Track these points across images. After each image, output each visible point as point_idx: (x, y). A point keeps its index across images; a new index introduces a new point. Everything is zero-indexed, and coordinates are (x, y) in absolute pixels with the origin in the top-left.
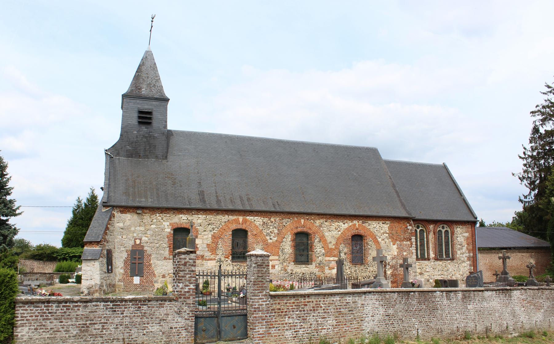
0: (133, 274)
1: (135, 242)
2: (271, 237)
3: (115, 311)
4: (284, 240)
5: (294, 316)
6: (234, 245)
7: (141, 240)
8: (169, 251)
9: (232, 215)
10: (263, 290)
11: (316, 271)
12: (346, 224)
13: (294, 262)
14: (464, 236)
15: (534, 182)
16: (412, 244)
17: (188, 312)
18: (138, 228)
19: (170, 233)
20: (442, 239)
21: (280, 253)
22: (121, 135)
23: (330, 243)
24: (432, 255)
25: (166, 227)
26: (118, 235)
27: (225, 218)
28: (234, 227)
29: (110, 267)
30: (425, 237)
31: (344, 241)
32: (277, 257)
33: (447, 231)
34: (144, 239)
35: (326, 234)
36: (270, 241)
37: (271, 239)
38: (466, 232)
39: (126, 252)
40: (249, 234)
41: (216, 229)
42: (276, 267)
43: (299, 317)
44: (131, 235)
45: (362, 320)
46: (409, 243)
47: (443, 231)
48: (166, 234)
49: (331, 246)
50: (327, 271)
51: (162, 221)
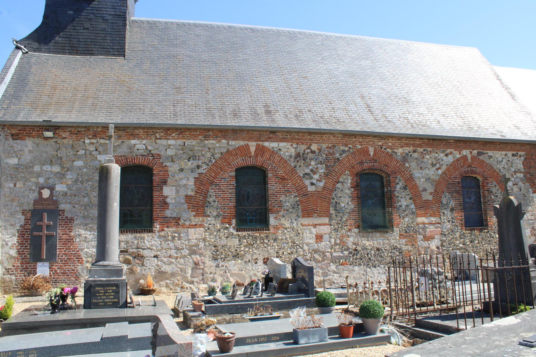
0: (37, 258)
1: (40, 194)
2: (314, 181)
4: (339, 185)
6: (241, 198)
7: (52, 189)
9: (234, 139)
11: (403, 244)
12: (450, 157)
13: (358, 227)
21: (332, 211)
22: (45, 17)
23: (425, 190)
26: (6, 181)
27: (221, 145)
28: (239, 162)
31: (448, 188)
32: (326, 220)
34: (60, 188)
37: (312, 184)
39: (23, 213)
40: (270, 175)
41: (205, 167)
42: (326, 237)
44: (33, 180)
49: (427, 196)
50: (421, 243)
51: (95, 153)
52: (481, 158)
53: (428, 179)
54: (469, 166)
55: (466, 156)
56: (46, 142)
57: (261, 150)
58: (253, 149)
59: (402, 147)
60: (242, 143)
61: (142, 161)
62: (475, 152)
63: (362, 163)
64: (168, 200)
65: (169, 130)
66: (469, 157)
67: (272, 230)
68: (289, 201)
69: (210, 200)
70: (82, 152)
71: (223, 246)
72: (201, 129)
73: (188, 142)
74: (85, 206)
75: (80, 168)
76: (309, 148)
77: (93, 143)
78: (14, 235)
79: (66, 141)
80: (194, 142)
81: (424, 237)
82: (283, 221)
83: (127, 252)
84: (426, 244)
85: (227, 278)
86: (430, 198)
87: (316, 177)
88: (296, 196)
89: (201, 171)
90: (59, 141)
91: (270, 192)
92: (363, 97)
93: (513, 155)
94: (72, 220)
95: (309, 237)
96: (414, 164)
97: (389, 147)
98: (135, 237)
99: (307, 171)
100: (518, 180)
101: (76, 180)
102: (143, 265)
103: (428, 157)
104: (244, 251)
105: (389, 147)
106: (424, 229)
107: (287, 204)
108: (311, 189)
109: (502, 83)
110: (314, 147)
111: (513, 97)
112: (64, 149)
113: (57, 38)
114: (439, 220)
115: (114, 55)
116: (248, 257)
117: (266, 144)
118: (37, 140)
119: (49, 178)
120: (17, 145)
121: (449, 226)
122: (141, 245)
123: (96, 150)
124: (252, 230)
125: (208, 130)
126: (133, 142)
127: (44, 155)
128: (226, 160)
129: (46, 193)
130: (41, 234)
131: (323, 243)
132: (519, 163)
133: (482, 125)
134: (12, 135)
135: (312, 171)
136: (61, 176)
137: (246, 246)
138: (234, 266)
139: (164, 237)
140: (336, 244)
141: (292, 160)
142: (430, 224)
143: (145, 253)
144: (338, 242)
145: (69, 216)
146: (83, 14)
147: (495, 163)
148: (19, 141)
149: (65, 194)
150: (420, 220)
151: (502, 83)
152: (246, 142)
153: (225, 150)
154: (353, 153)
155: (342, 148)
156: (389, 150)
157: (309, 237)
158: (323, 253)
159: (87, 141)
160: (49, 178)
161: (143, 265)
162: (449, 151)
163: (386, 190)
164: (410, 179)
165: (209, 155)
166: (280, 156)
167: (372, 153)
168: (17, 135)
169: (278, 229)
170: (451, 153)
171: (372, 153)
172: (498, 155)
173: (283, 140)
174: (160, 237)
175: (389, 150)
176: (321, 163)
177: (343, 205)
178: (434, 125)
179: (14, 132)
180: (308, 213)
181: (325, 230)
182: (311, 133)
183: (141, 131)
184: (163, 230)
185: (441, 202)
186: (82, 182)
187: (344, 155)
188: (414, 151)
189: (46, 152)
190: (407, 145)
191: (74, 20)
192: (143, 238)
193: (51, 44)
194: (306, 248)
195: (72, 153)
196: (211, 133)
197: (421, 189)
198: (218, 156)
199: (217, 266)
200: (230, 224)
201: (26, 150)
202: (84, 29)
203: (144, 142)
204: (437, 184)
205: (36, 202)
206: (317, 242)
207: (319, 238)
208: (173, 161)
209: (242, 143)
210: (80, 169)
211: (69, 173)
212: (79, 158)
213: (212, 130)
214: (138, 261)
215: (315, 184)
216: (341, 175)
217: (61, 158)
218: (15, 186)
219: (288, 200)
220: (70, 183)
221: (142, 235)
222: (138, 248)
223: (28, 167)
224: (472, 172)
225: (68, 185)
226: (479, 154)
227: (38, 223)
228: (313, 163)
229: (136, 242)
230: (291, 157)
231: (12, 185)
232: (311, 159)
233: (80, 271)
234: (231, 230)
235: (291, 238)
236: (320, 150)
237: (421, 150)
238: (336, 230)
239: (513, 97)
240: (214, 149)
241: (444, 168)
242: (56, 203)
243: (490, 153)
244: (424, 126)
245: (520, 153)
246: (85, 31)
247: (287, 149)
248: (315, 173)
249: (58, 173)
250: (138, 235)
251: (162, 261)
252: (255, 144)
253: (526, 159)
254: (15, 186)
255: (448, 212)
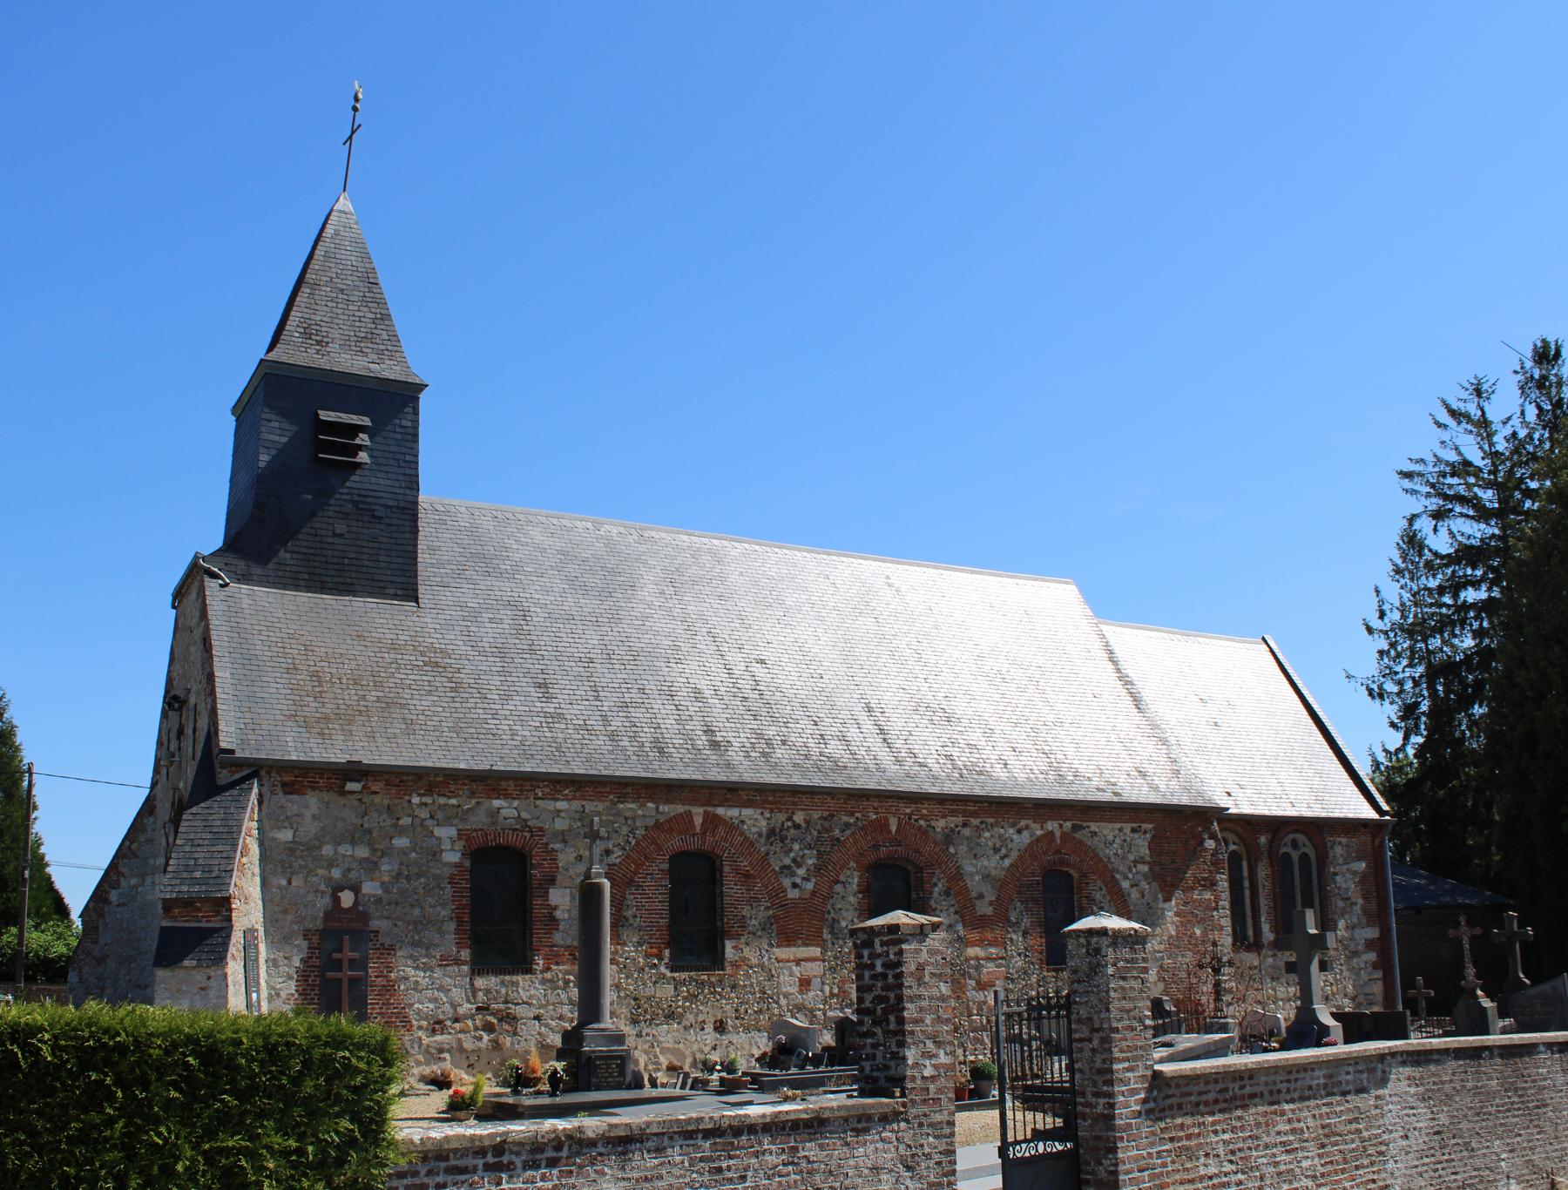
1: (337, 900)
2: (798, 881)
3: (719, 1170)
4: (838, 888)
5: (1221, 1151)
7: (356, 889)
8: (458, 931)
9: (668, 802)
10: (1135, 1058)
12: (1025, 834)
14: (1355, 873)
15: (1417, 705)
16: (1217, 899)
17: (937, 1158)
18: (346, 850)
19: (456, 865)
20: (1293, 881)
21: (827, 936)
23: (981, 896)
24: (1268, 935)
25: (446, 845)
27: (648, 812)
28: (675, 843)
29: (254, 996)
30: (1246, 874)
31: (1019, 892)
32: (816, 951)
33: (1304, 857)
34: (369, 888)
35: (968, 868)
36: (793, 894)
37: (795, 885)
38: (1360, 859)
40: (727, 869)
42: (816, 982)
43: (1233, 1152)
44: (321, 872)
45: (1381, 1153)
46: (1208, 895)
47: (1295, 856)
48: (447, 872)
49: (984, 908)
51: (429, 823)
52: (1077, 835)
53: (986, 877)
54: (1058, 852)
55: (1052, 833)
56: (342, 801)
57: (712, 822)
58: (698, 821)
59: (944, 816)
60: (680, 809)
61: (511, 839)
62: (1068, 824)
63: (876, 847)
64: (558, 914)
65: (560, 784)
66: (1058, 834)
67: (729, 970)
68: (756, 915)
69: (629, 913)
70: (406, 821)
71: (649, 999)
72: (612, 783)
73: (590, 806)
74: (416, 923)
75: (404, 852)
76: (790, 819)
77: (426, 804)
78: (290, 978)
79: (377, 799)
80: (601, 806)
81: (978, 982)
82: (747, 952)
83: (487, 1009)
84: (980, 996)
85: (656, 1056)
86: (989, 911)
87: (801, 872)
88: (767, 908)
89: (612, 859)
90: (367, 799)
91: (727, 900)
92: (869, 709)
93: (1133, 830)
94: (392, 948)
95: (788, 983)
96: (963, 848)
97: (922, 817)
98: (502, 982)
99: (787, 861)
100: (1139, 877)
101: (399, 875)
102: (515, 1034)
103: (987, 834)
104: (683, 1007)
105: (922, 817)
106: (978, 968)
107: (754, 922)
108: (793, 894)
109: (1118, 670)
110: (799, 818)
111: (1137, 701)
112: (375, 815)
113: (282, 554)
114: (1003, 953)
115: (395, 597)
116: (690, 1018)
117: (720, 811)
118: (326, 796)
119: (349, 870)
120: (292, 804)
121: (1019, 962)
122: (513, 995)
123: (432, 817)
124: (697, 969)
125: (626, 785)
126: (496, 803)
127: (340, 824)
128: (654, 842)
129: (347, 899)
130: (340, 975)
131: (812, 994)
132: (1142, 846)
133: (1082, 768)
134: (284, 785)
135: (794, 860)
136: (371, 866)
137: (685, 999)
138: (667, 1033)
139: (550, 981)
140: (832, 995)
141: (763, 840)
142: (988, 959)
143: (520, 1011)
144: (836, 991)
145: (388, 942)
146: (332, 502)
147: (1102, 845)
148: (294, 797)
149: (379, 900)
150: (972, 951)
151: (1118, 670)
152: (687, 808)
153: (651, 822)
154: (863, 828)
155: (845, 819)
156: (922, 822)
157: (788, 983)
158: (811, 1011)
159: (416, 800)
160: (349, 870)
161: (515, 1034)
162: (1023, 823)
163: (914, 895)
164: (957, 877)
165: (625, 830)
166: (742, 834)
167: (894, 829)
168: (293, 783)
169: (738, 967)
170: (1027, 827)
171: (894, 829)
172: (1107, 830)
173: (748, 804)
174: (544, 981)
175: (922, 822)
176: (810, 847)
177: (844, 924)
178: (999, 772)
179: (286, 779)
180: (788, 938)
181: (815, 969)
182: (795, 791)
183: (511, 783)
184: (549, 969)
185: (1008, 920)
186: (408, 878)
187: (848, 832)
188: (965, 825)
189: (343, 820)
190: (954, 813)
191: (313, 515)
192: (516, 984)
193: (271, 566)
194: (783, 1001)
195: (389, 822)
196: (629, 790)
197: (974, 894)
198: (640, 832)
199: (639, 1035)
200: (661, 959)
201: (308, 814)
202: (336, 535)
203: (516, 803)
204: (1001, 885)
205: (328, 915)
206: (801, 992)
207: (805, 984)
208: (565, 841)
209: (680, 809)
210: (405, 853)
211: (385, 860)
212: (402, 831)
213: (632, 784)
214: (506, 1027)
215: (799, 886)
216: (842, 868)
217: (370, 832)
218: (289, 883)
219: (756, 915)
220: (386, 879)
221: (515, 978)
222: (506, 1002)
223: (312, 847)
224: (1062, 862)
225: (383, 884)
226: (1075, 828)
227: (336, 956)
228: (796, 847)
229: (503, 991)
230: (760, 835)
231: (284, 882)
232: (793, 840)
233: (407, 1045)
234: (663, 969)
235: (759, 983)
236: (808, 822)
237: (975, 822)
238: (833, 969)
239: (1137, 701)
240: (634, 819)
241: (1015, 854)
242: (364, 917)
243: (1094, 827)
244: (980, 773)
245: (1144, 826)
246: (337, 540)
247: (754, 820)
248: (799, 866)
249: (365, 859)
250: (507, 978)
251: (547, 1026)
252: (701, 810)
253: (1154, 837)
254: (289, 883)
255: (1017, 937)
